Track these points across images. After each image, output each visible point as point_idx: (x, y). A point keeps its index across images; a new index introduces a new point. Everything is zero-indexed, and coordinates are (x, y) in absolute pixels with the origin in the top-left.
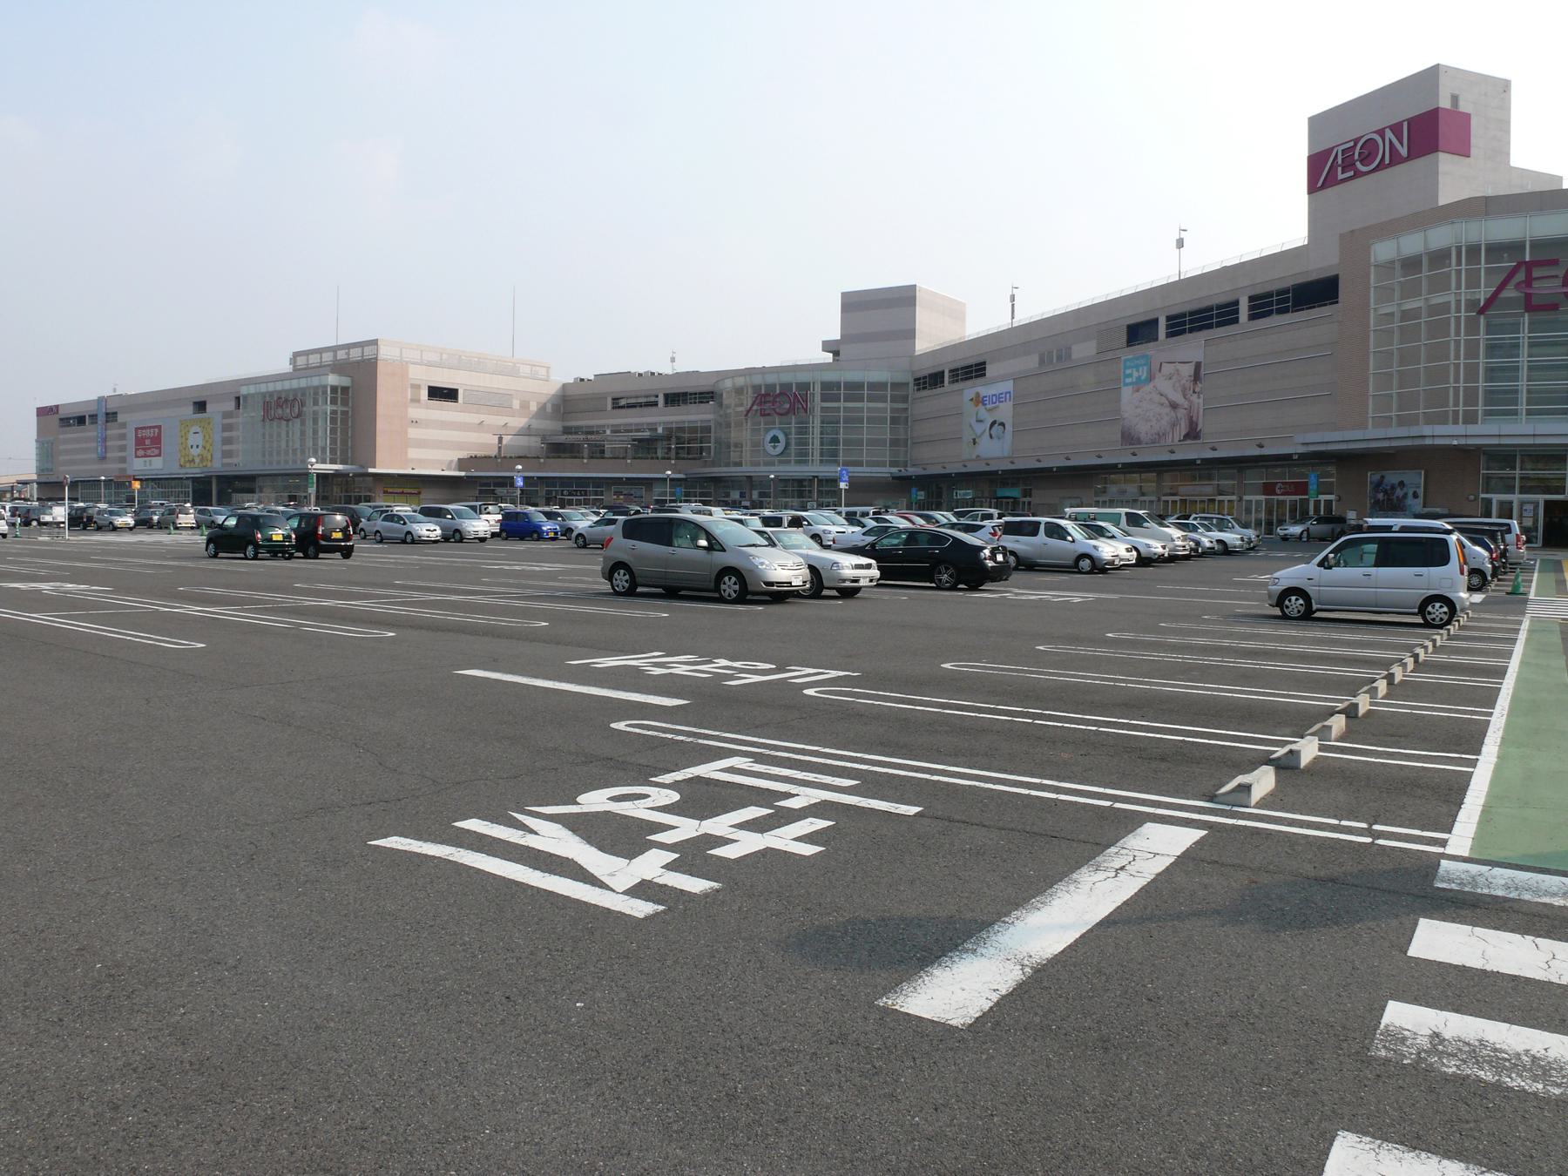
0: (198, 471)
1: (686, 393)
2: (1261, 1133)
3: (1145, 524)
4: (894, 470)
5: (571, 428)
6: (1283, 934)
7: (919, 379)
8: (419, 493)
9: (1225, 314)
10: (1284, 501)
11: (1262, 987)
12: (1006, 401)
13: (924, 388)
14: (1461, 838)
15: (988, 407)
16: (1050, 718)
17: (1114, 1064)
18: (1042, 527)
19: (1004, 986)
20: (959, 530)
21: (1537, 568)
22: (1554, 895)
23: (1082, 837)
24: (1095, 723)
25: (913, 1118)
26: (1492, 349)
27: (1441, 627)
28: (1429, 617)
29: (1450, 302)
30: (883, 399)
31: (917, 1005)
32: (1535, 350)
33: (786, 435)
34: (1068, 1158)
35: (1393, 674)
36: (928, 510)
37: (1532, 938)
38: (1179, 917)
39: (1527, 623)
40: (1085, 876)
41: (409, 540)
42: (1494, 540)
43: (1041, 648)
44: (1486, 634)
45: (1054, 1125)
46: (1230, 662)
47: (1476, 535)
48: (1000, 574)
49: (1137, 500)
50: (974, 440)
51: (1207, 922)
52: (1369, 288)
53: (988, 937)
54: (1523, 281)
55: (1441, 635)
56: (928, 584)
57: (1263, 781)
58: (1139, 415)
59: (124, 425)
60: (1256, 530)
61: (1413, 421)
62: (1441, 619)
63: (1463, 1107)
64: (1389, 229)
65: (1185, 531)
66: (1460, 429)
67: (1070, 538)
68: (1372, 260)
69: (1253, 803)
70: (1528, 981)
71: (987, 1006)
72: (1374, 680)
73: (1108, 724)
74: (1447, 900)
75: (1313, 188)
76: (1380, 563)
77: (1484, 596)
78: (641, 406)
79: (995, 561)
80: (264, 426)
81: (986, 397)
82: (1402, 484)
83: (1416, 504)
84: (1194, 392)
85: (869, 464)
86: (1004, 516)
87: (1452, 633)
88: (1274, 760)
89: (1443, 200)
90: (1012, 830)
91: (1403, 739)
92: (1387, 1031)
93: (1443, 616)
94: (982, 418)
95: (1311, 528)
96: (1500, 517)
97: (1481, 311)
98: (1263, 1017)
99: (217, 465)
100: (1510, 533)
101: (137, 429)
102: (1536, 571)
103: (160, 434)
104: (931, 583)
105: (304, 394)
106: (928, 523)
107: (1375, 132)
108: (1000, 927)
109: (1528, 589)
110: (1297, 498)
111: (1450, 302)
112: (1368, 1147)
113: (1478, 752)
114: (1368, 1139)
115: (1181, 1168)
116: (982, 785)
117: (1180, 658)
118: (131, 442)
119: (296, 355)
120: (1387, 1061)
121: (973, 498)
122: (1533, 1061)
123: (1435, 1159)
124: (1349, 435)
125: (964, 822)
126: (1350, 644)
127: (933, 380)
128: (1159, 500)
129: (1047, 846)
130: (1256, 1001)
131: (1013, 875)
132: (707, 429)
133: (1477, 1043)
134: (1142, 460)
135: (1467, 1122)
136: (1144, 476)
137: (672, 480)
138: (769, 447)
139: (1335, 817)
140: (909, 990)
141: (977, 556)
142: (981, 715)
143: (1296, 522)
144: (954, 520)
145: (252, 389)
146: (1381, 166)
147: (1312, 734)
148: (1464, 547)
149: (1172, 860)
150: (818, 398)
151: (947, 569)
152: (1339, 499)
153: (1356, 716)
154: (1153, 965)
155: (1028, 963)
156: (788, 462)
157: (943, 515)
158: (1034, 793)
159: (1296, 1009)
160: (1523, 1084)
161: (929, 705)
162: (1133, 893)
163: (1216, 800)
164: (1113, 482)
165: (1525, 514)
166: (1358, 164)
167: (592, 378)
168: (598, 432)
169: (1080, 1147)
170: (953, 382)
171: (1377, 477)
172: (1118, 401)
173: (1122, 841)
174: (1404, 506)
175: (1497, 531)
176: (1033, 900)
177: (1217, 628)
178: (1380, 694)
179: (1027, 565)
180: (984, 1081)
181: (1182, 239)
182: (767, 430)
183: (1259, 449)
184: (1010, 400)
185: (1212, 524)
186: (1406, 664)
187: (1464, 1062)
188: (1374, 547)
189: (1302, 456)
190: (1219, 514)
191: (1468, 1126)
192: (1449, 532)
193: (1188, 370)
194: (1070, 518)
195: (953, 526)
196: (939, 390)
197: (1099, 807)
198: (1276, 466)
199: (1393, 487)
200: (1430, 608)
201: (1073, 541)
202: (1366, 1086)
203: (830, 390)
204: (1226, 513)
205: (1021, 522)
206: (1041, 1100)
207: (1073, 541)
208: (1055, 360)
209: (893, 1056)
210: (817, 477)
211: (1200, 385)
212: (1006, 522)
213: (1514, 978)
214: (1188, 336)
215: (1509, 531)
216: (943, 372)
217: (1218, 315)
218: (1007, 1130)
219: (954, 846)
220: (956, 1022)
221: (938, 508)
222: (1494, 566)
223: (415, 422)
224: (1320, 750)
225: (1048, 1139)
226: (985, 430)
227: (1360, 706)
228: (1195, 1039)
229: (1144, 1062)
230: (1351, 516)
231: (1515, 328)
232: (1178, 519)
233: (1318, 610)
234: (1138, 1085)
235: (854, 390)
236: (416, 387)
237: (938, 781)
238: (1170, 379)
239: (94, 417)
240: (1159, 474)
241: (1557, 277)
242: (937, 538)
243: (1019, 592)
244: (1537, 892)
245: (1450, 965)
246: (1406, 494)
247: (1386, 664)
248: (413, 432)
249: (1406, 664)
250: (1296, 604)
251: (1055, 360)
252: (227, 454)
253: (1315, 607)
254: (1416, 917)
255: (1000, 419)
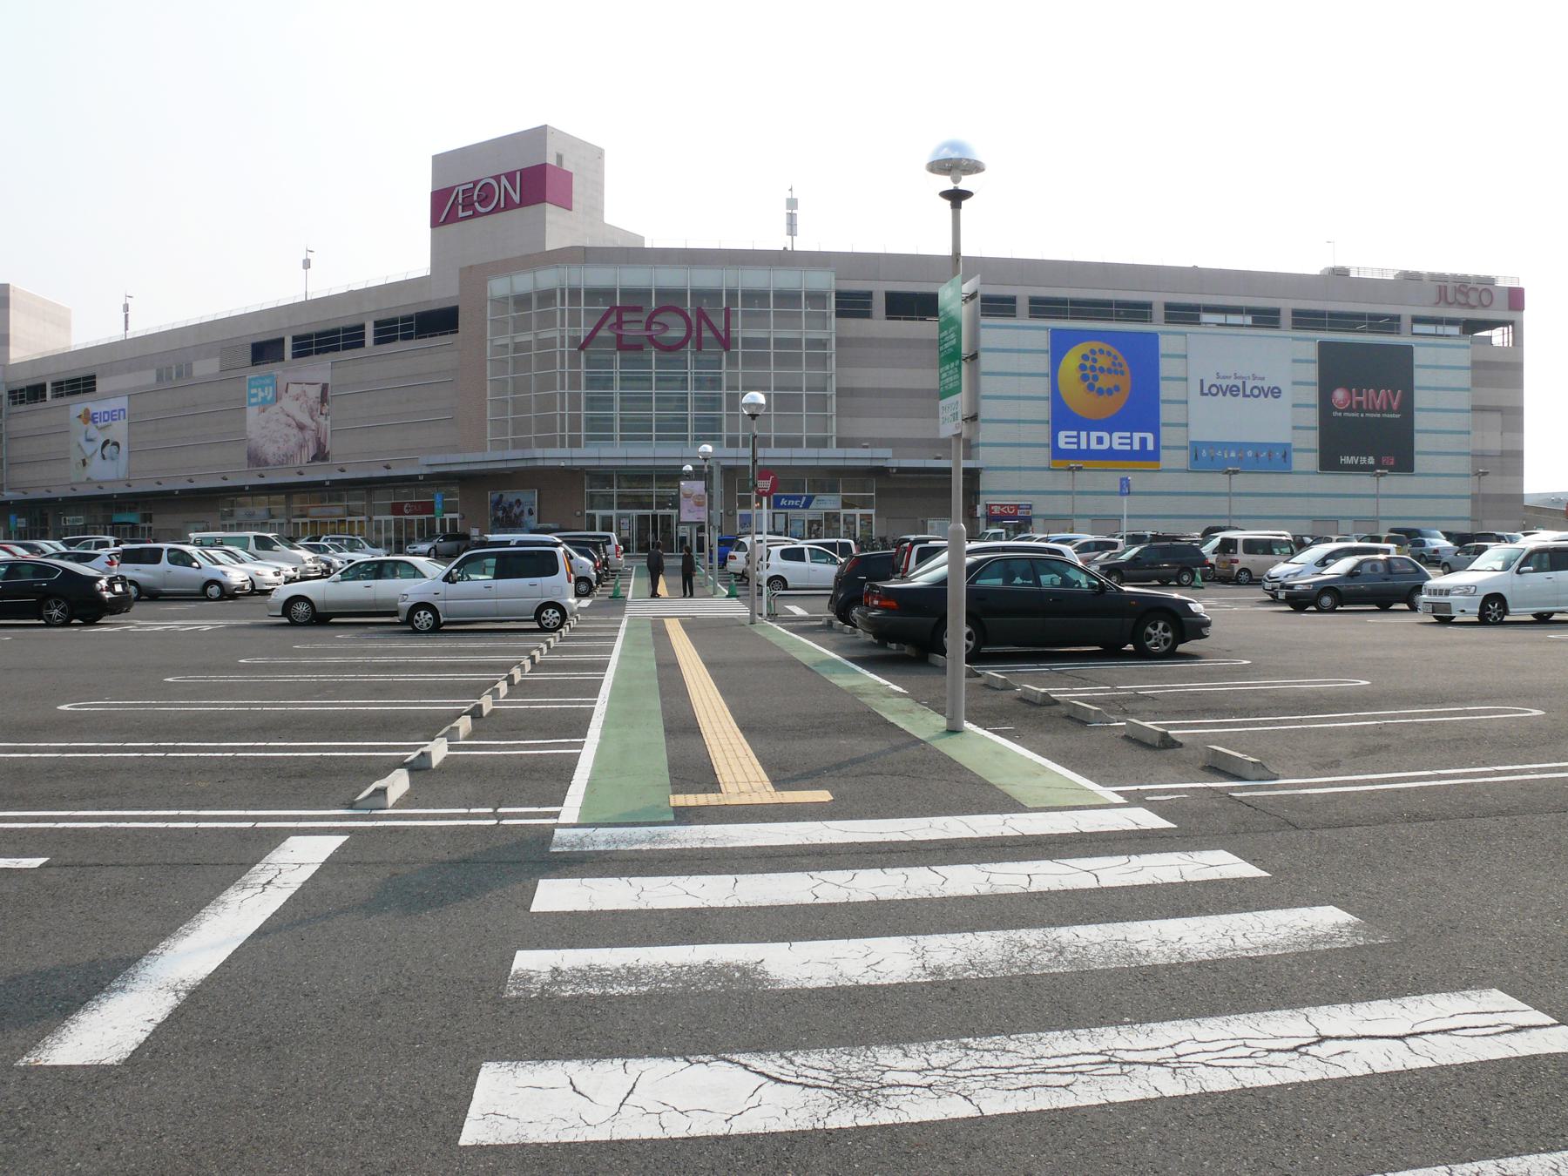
2: (418, 1082)
3: (275, 548)
6: (423, 915)
9: (350, 337)
10: (413, 521)
11: (409, 963)
13: (22, 402)
14: (571, 809)
15: (99, 424)
16: (184, 749)
17: (278, 1059)
18: (165, 554)
19: (159, 1014)
20: (70, 560)
21: (633, 574)
22: (643, 842)
23: (226, 860)
24: (232, 749)
25: (73, 1164)
26: (592, 381)
27: (554, 630)
28: (544, 623)
29: (555, 338)
31: (64, 1055)
32: (627, 384)
34: (242, 1153)
35: (513, 676)
36: (31, 539)
37: (626, 878)
38: (327, 916)
39: (626, 622)
40: (233, 896)
42: (598, 551)
43: (170, 680)
44: (592, 634)
45: (226, 1127)
46: (364, 678)
47: (583, 547)
48: (119, 606)
49: (266, 523)
50: (84, 461)
51: (354, 917)
52: (486, 321)
53: (137, 972)
54: (615, 324)
55: (554, 637)
56: (36, 622)
57: (398, 784)
58: (266, 436)
60: (386, 549)
61: (525, 444)
62: (555, 624)
63: (578, 1019)
64: (506, 267)
65: (316, 553)
66: (566, 452)
67: (195, 564)
68: (489, 294)
69: (390, 805)
70: (624, 912)
71: (142, 1037)
72: (497, 682)
73: (245, 749)
74: (561, 861)
75: (435, 223)
76: (499, 575)
77: (590, 601)
79: (114, 593)
81: (97, 414)
82: (518, 502)
83: (532, 521)
84: (321, 414)
86: (122, 543)
87: (564, 635)
88: (407, 763)
89: (552, 244)
90: (151, 864)
91: (522, 732)
92: (517, 976)
93: (556, 620)
94: (92, 437)
95: (438, 545)
96: (603, 530)
97: (582, 347)
98: (411, 988)
100: (610, 544)
102: (633, 576)
104: (39, 620)
106: (32, 553)
107: (491, 177)
108: (148, 959)
109: (625, 593)
110: (424, 517)
111: (555, 338)
112: (506, 1069)
113: (585, 736)
114: (506, 1063)
115: (350, 1130)
116: (114, 825)
117: (314, 678)
120: (518, 999)
121: (86, 525)
122: (628, 972)
123: (559, 1063)
124: (470, 457)
125: (97, 865)
126: (474, 652)
127: (34, 393)
128: (289, 522)
129: (191, 874)
130: (404, 976)
131: (157, 908)
133: (587, 968)
134: (269, 482)
135: (581, 1029)
136: (273, 498)
139: (465, 807)
140: (53, 1042)
141: (93, 588)
142: (108, 755)
143: (424, 541)
144: (63, 549)
146: (496, 210)
147: (442, 736)
148: (571, 557)
149: (317, 867)
151: (57, 603)
152: (463, 518)
153: (481, 716)
154: (306, 964)
155: (181, 988)
157: (49, 544)
158: (172, 825)
159: (439, 974)
160: (621, 990)
161: (46, 751)
162: (282, 904)
163: (357, 805)
164: (241, 505)
165: (622, 527)
166: (476, 204)
169: (253, 1140)
170: (57, 396)
171: (496, 496)
172: (244, 420)
173: (266, 858)
174: (521, 522)
175: (599, 543)
176: (181, 928)
177: (351, 646)
178: (502, 695)
179: (150, 595)
180: (149, 1108)
181: (309, 260)
183: (386, 470)
184: (125, 418)
185: (343, 545)
186: (524, 665)
187: (578, 984)
188: (492, 562)
189: (427, 476)
190: (349, 534)
191: (582, 1032)
192: (557, 545)
193: (315, 392)
194: (195, 544)
195: (62, 556)
196: (40, 405)
197: (241, 829)
198: (403, 487)
199: (511, 505)
200: (544, 615)
201: (200, 567)
202: (501, 1023)
204: (356, 533)
205: (141, 549)
206: (210, 1109)
207: (200, 567)
208: (174, 377)
209: (43, 1111)
211: (328, 407)
212: (124, 550)
213: (614, 912)
214: (314, 357)
215: (609, 542)
217: (345, 338)
218: (178, 1146)
219: (89, 890)
220: (112, 1059)
221: (44, 536)
222: (597, 574)
224: (449, 750)
225: (222, 1141)
226: (95, 452)
227: (484, 707)
228: (351, 1020)
229: (306, 1050)
230: (474, 532)
231: (610, 364)
232: (308, 540)
233: (446, 623)
234: (303, 1072)
237: (64, 828)
238: (297, 399)
240: (289, 497)
241: (641, 321)
242: (43, 570)
243: (142, 623)
244: (629, 842)
245: (565, 912)
246: (523, 511)
247: (507, 667)
249: (524, 665)
250: (424, 618)
251: (174, 377)
253: (442, 620)
254: (536, 879)
255: (113, 438)
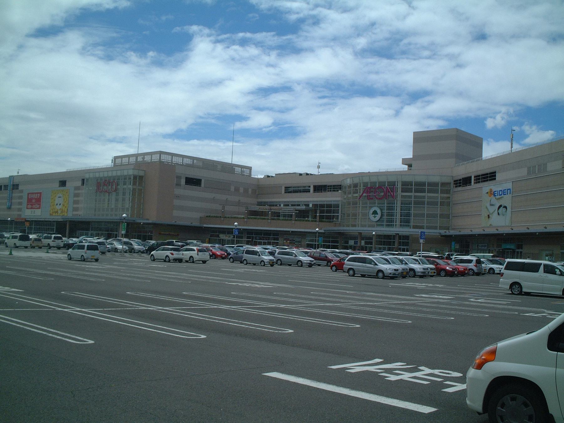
0: (60, 217)
1: (326, 185)
4: (443, 232)
5: (262, 202)
7: (457, 181)
8: (178, 235)
12: (507, 194)
13: (460, 186)
15: (497, 197)
30: (436, 191)
33: (381, 210)
41: (167, 260)
50: (489, 216)
59: (22, 191)
78: (301, 192)
80: (96, 196)
81: (496, 191)
85: (441, 228)
94: (493, 204)
99: (70, 215)
101: (28, 194)
103: (40, 196)
105: (118, 179)
118: (25, 200)
119: (116, 158)
132: (337, 206)
137: (319, 233)
138: (371, 217)
145: (91, 175)
150: (399, 190)
156: (382, 225)
167: (274, 175)
168: (276, 205)
182: (371, 207)
196: (468, 187)
203: (407, 186)
210: (398, 234)
216: (471, 177)
223: (178, 197)
235: (420, 186)
236: (179, 178)
239: (6, 187)
248: (177, 202)
252: (75, 209)
